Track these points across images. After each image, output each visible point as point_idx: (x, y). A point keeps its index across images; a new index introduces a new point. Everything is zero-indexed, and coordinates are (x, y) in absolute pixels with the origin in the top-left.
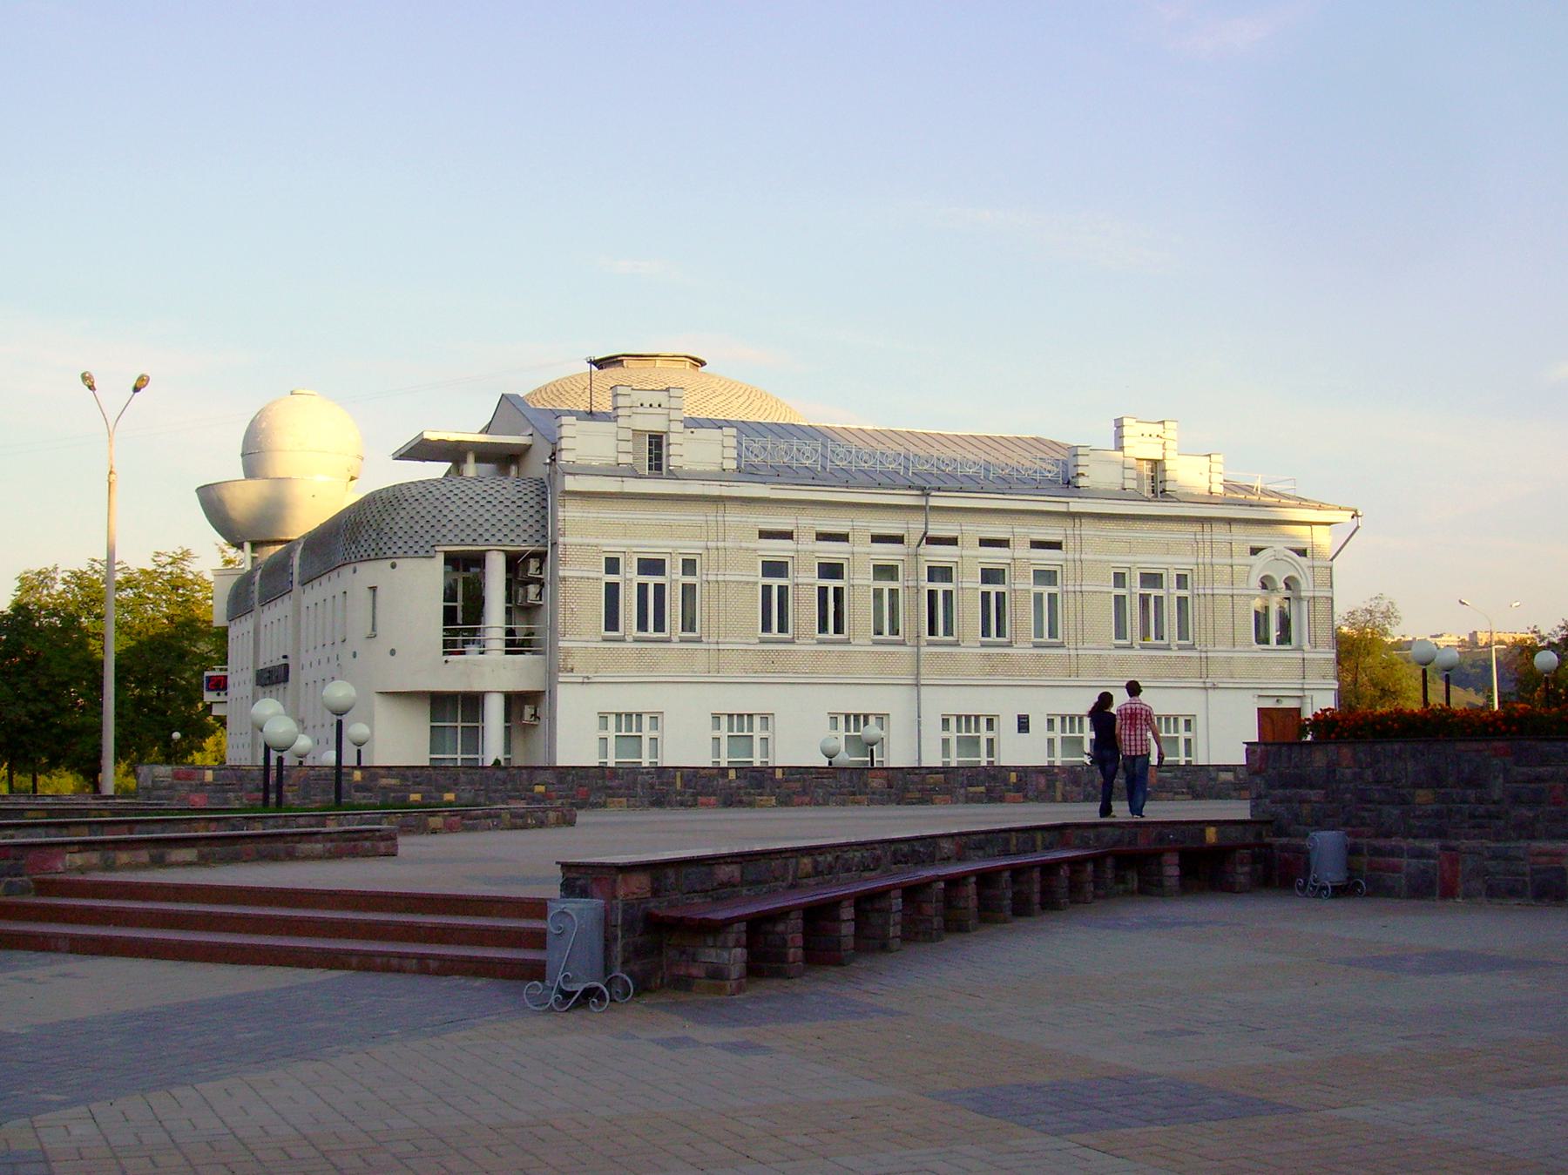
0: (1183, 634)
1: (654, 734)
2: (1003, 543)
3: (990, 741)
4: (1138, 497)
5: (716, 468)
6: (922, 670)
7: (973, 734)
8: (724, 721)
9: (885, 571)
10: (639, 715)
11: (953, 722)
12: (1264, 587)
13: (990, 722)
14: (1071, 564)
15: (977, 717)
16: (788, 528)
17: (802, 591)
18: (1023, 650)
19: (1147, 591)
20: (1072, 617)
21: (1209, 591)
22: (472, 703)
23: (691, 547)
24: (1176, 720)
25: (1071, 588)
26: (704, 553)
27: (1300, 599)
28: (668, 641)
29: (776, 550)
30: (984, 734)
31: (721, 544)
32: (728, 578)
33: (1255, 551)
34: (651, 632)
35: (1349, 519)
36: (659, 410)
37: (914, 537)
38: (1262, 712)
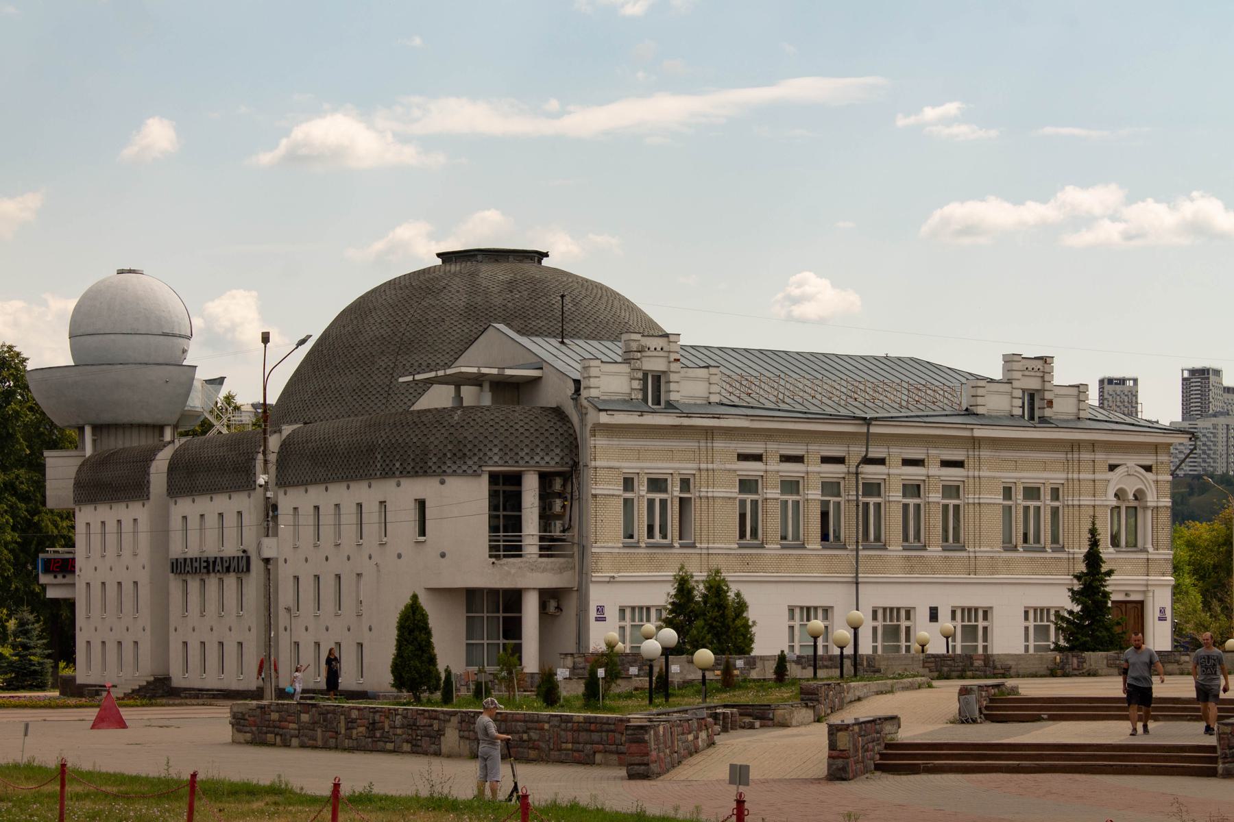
0: (1055, 540)
3: (985, 629)
6: (860, 570)
7: (973, 623)
9: (913, 489)
10: (648, 609)
14: (971, 480)
15: (898, 609)
17: (770, 505)
18: (935, 551)
20: (971, 527)
21: (1076, 503)
22: (513, 599)
23: (688, 468)
25: (971, 501)
27: (1145, 508)
28: (671, 546)
29: (751, 469)
31: (710, 466)
32: (716, 494)
33: (1112, 468)
36: (662, 354)
37: (853, 461)
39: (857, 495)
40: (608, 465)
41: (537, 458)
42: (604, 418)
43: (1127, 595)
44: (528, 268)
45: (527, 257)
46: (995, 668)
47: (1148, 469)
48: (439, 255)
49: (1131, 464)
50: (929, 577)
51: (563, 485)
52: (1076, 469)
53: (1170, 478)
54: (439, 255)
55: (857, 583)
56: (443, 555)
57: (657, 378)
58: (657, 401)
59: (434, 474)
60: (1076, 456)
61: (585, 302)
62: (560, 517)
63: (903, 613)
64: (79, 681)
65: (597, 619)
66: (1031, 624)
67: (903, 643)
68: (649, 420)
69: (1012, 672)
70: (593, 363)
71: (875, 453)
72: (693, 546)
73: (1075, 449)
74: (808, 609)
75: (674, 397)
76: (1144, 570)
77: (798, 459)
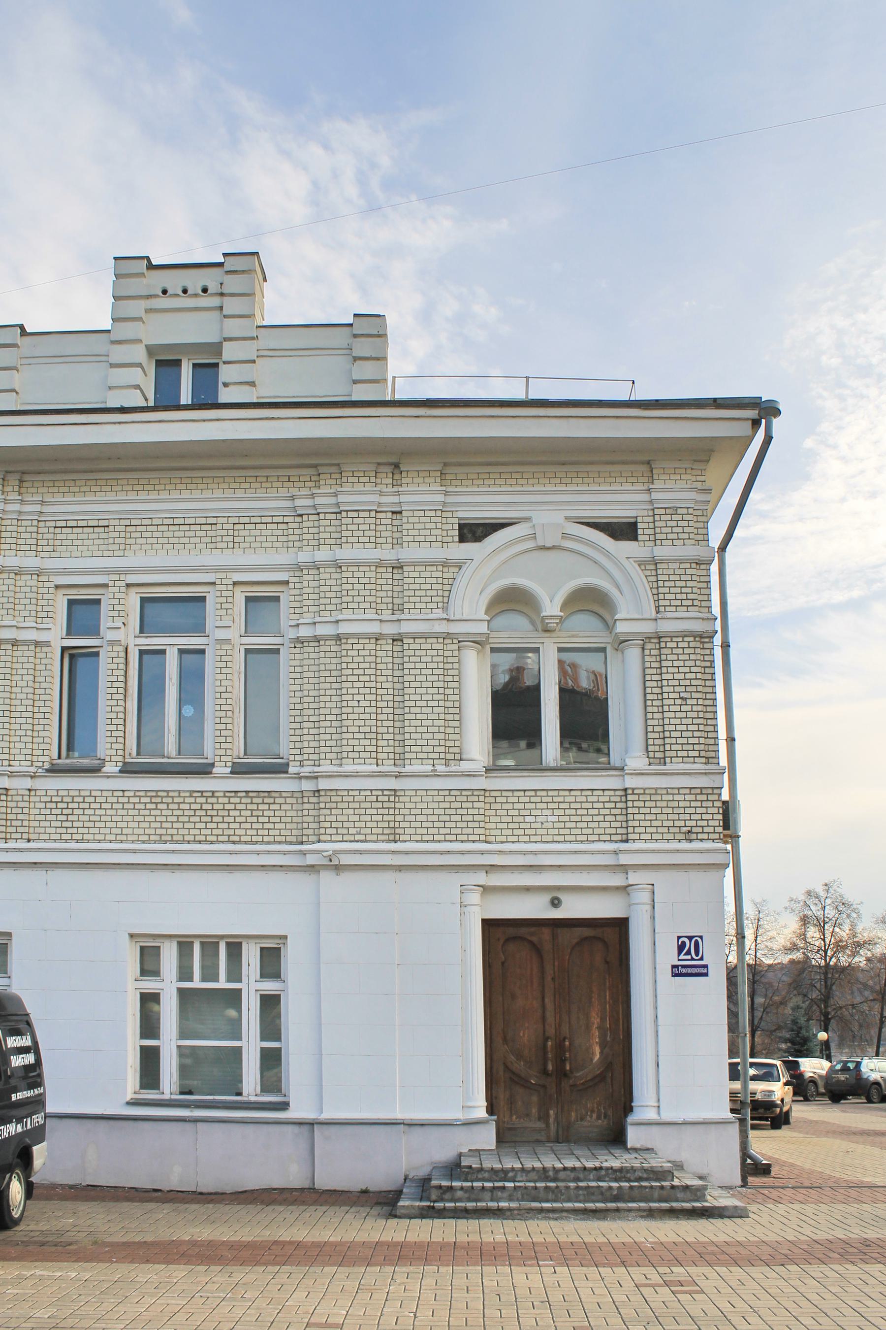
3: (270, 1004)
7: (222, 983)
23: (264, 558)
24: (235, 948)
30: (252, 986)
33: (473, 532)
43: (555, 903)
47: (624, 531)
49: (541, 517)
63: (251, 957)
65: (677, 972)
66: (168, 986)
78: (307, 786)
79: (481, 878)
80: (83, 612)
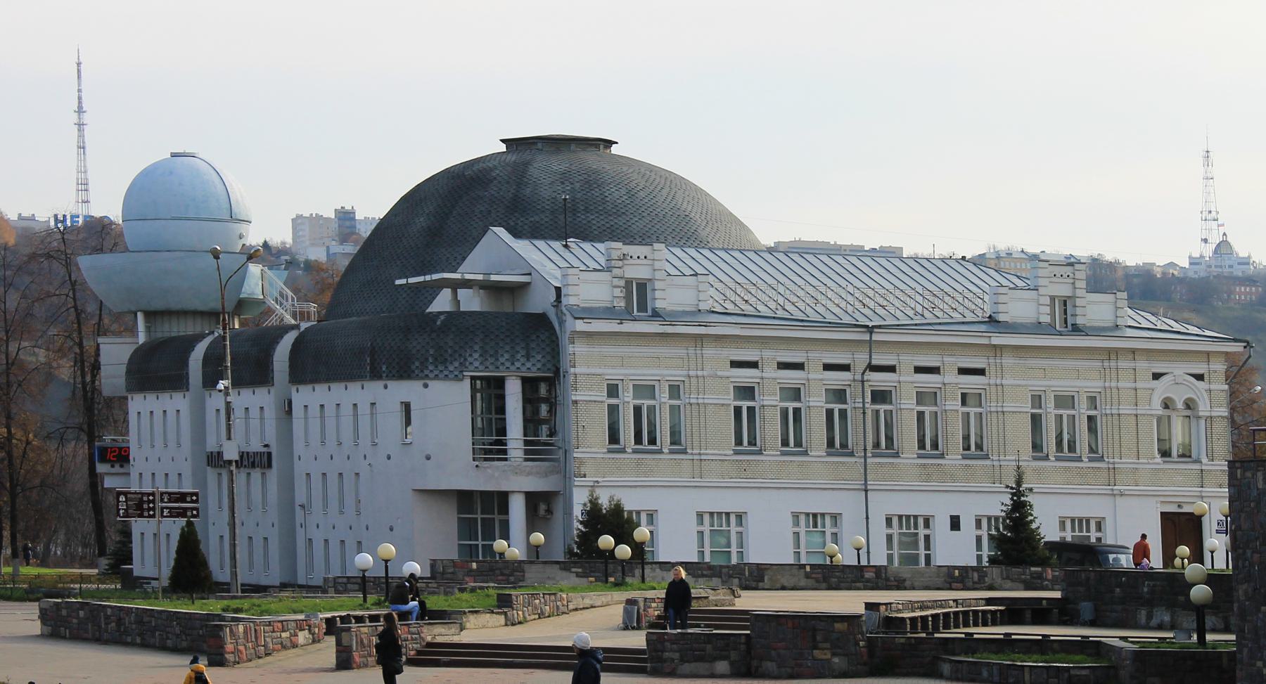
1: (835, 530)
2: (799, 366)
3: (927, 538)
4: (1049, 330)
5: (1034, 321)
7: (912, 531)
8: (707, 518)
9: (839, 395)
10: (728, 514)
11: (895, 521)
12: (1166, 407)
13: (740, 517)
14: (993, 388)
15: (916, 517)
16: (937, 364)
17: (905, 414)
19: (1061, 412)
21: (1114, 412)
22: (500, 500)
23: (676, 374)
24: (1088, 521)
26: (687, 380)
28: (660, 452)
30: (922, 532)
31: (700, 373)
33: (1157, 376)
34: (645, 445)
35: (1241, 349)
36: (645, 262)
38: (1164, 515)
39: (864, 402)
40: (591, 371)
41: (518, 364)
42: (580, 326)
44: (591, 159)
45: (591, 145)
46: (887, 579)
47: (1200, 377)
48: (503, 141)
50: (949, 485)
51: (544, 394)
52: (1114, 375)
53: (1226, 387)
54: (503, 141)
55: (866, 491)
56: (428, 458)
57: (642, 286)
58: (642, 306)
59: (417, 378)
60: (1113, 364)
61: (642, 194)
62: (545, 421)
63: (921, 521)
64: (135, 574)
66: (706, 528)
67: (922, 552)
68: (629, 327)
69: (908, 583)
70: (571, 271)
71: (878, 360)
72: (684, 452)
73: (1113, 356)
74: (815, 515)
75: (659, 304)
76: (1198, 482)
77: (799, 366)
78: (696, 457)
79: (1162, 499)
80: (1037, 400)
